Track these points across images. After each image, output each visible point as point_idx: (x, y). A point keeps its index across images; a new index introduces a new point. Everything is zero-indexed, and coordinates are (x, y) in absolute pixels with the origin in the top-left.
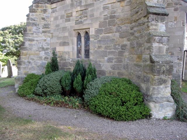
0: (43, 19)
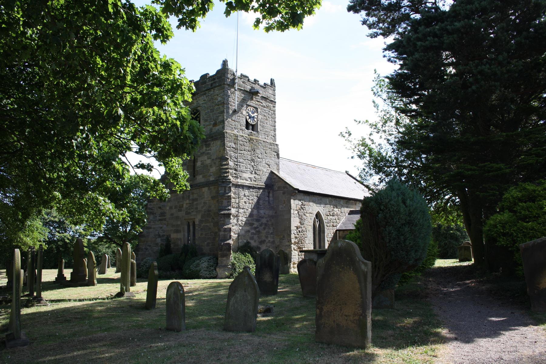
0: (160, 208)
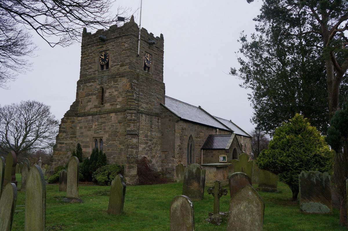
0: (71, 128)
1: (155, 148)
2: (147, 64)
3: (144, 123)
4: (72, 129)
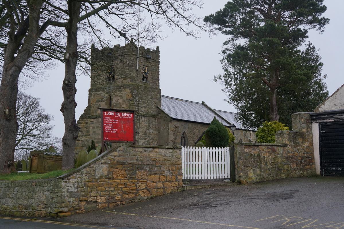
0: (86, 128)
1: (153, 143)
2: (145, 75)
3: (143, 123)
4: (86, 129)
